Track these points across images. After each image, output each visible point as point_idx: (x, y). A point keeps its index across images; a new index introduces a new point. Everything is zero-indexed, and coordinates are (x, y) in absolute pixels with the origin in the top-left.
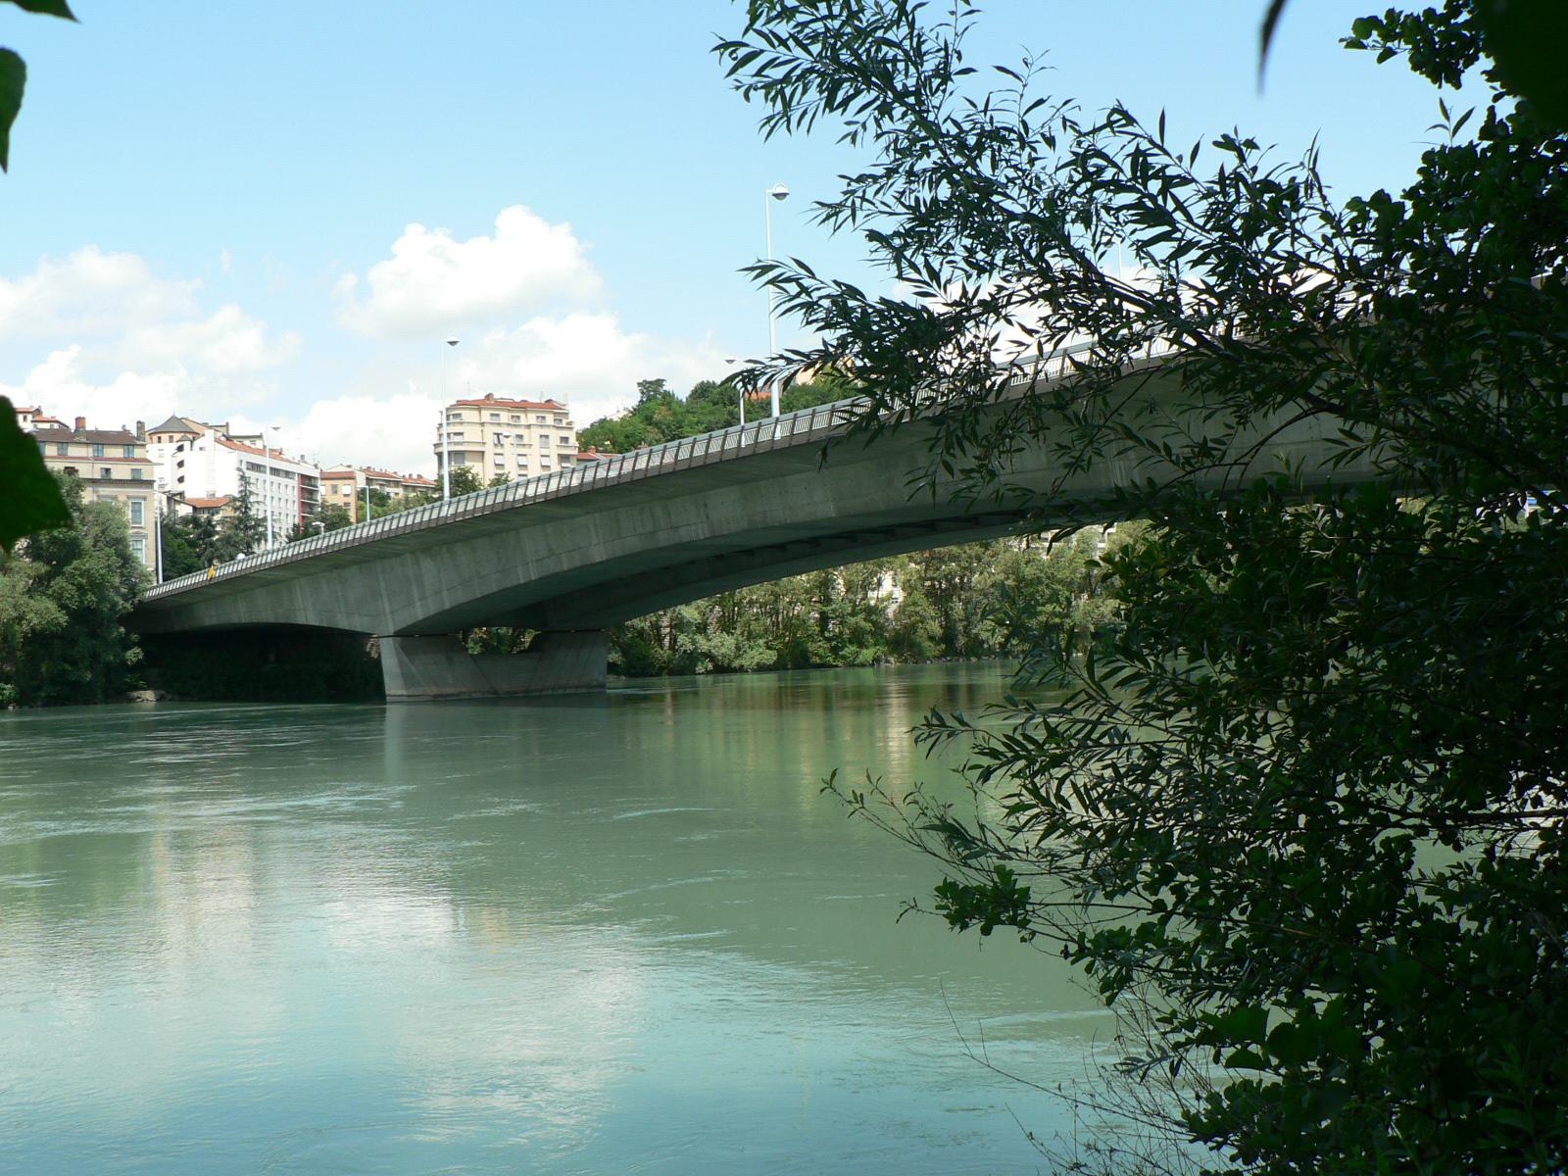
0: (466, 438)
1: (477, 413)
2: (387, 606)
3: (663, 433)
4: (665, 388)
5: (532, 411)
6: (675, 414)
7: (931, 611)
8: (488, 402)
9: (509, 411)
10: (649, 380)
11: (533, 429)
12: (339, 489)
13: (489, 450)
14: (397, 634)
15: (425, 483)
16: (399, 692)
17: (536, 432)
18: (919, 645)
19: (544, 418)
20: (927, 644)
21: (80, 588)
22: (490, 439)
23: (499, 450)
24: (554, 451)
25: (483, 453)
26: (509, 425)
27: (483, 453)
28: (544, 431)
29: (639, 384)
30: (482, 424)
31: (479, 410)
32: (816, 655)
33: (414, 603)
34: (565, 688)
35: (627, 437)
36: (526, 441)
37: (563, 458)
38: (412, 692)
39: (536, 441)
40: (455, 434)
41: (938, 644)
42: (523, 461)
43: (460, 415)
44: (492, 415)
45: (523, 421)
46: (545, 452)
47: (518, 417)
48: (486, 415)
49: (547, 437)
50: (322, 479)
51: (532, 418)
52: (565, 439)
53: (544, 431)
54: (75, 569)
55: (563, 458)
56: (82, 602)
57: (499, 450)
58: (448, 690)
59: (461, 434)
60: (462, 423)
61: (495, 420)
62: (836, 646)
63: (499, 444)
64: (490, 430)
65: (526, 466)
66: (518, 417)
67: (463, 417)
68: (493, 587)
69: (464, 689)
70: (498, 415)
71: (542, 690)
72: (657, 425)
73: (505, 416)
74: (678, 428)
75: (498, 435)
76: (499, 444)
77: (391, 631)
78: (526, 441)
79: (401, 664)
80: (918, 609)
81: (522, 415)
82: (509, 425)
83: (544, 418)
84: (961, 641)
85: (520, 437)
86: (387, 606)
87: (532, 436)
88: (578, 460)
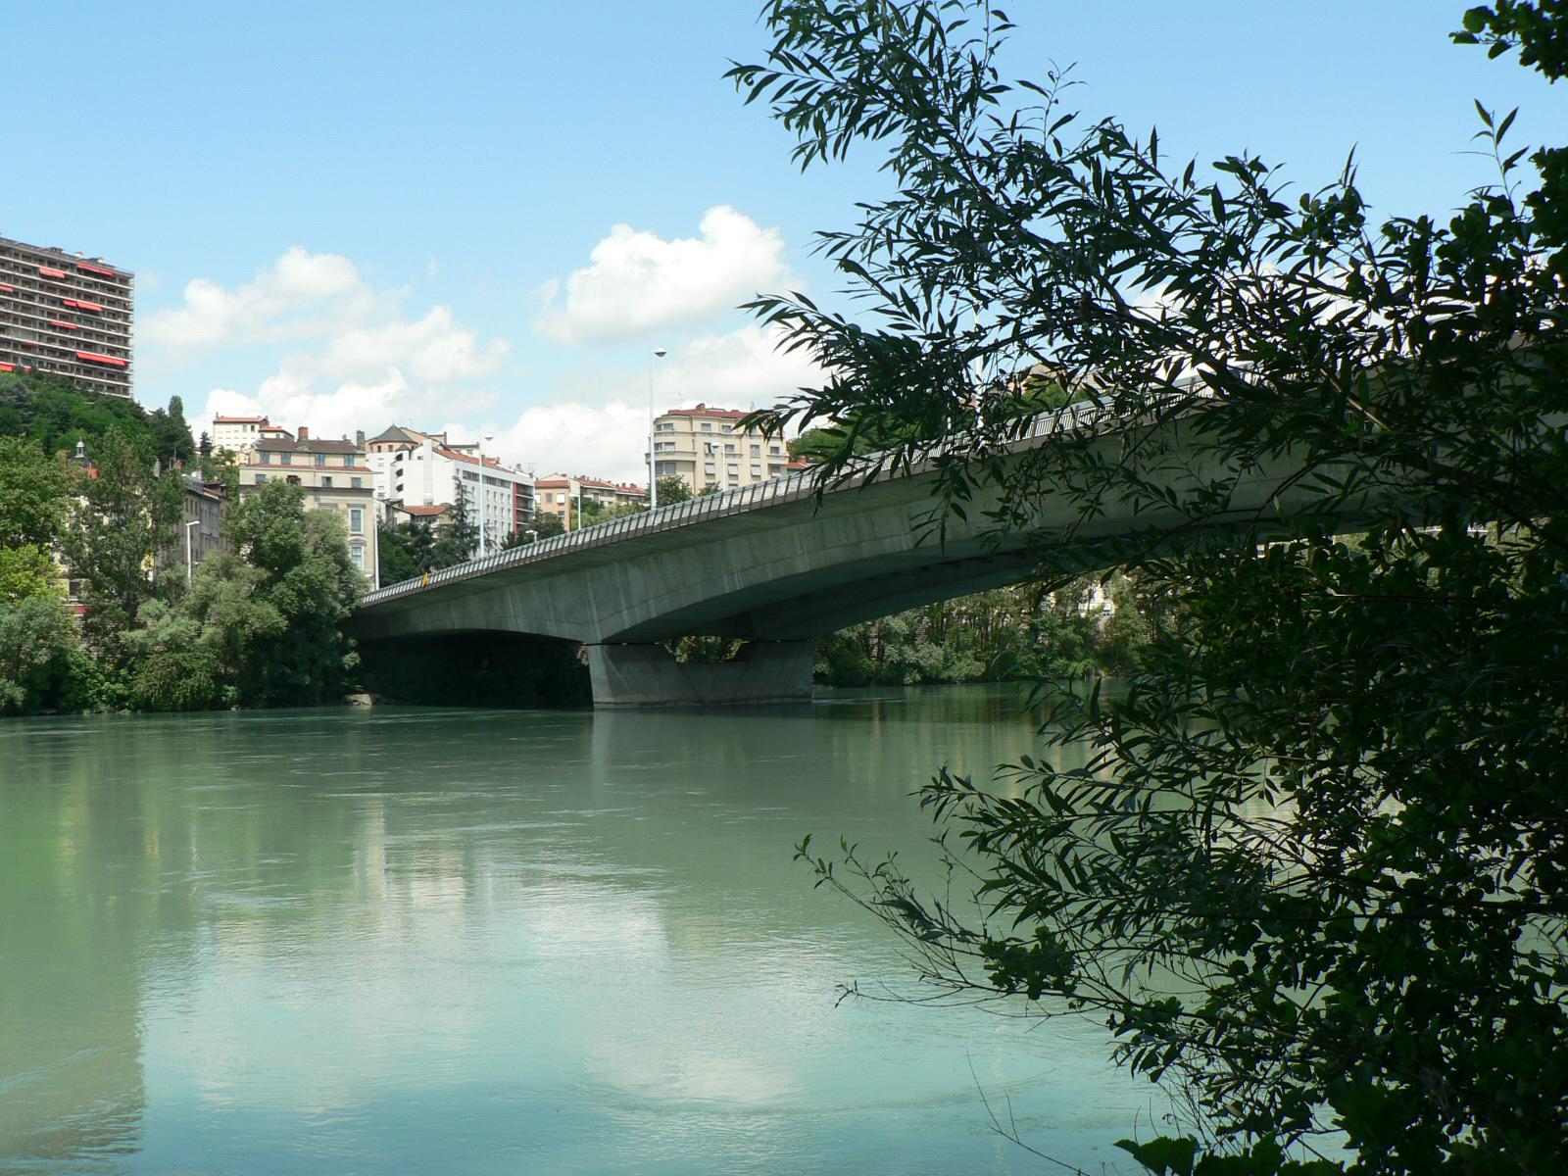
0: (678, 448)
1: (688, 423)
5: (698, 419)
9: (720, 421)
13: (700, 460)
22: (701, 448)
23: (710, 460)
24: (764, 461)
26: (719, 434)
30: (694, 434)
31: (691, 420)
37: (773, 468)
40: (667, 444)
42: (733, 470)
44: (703, 425)
46: (756, 461)
48: (697, 425)
49: (758, 447)
56: (301, 607)
57: (710, 460)
58: (654, 698)
59: (673, 444)
64: (701, 440)
69: (667, 697)
76: (710, 453)
77: (600, 639)
79: (608, 672)
82: (719, 434)
85: (732, 446)
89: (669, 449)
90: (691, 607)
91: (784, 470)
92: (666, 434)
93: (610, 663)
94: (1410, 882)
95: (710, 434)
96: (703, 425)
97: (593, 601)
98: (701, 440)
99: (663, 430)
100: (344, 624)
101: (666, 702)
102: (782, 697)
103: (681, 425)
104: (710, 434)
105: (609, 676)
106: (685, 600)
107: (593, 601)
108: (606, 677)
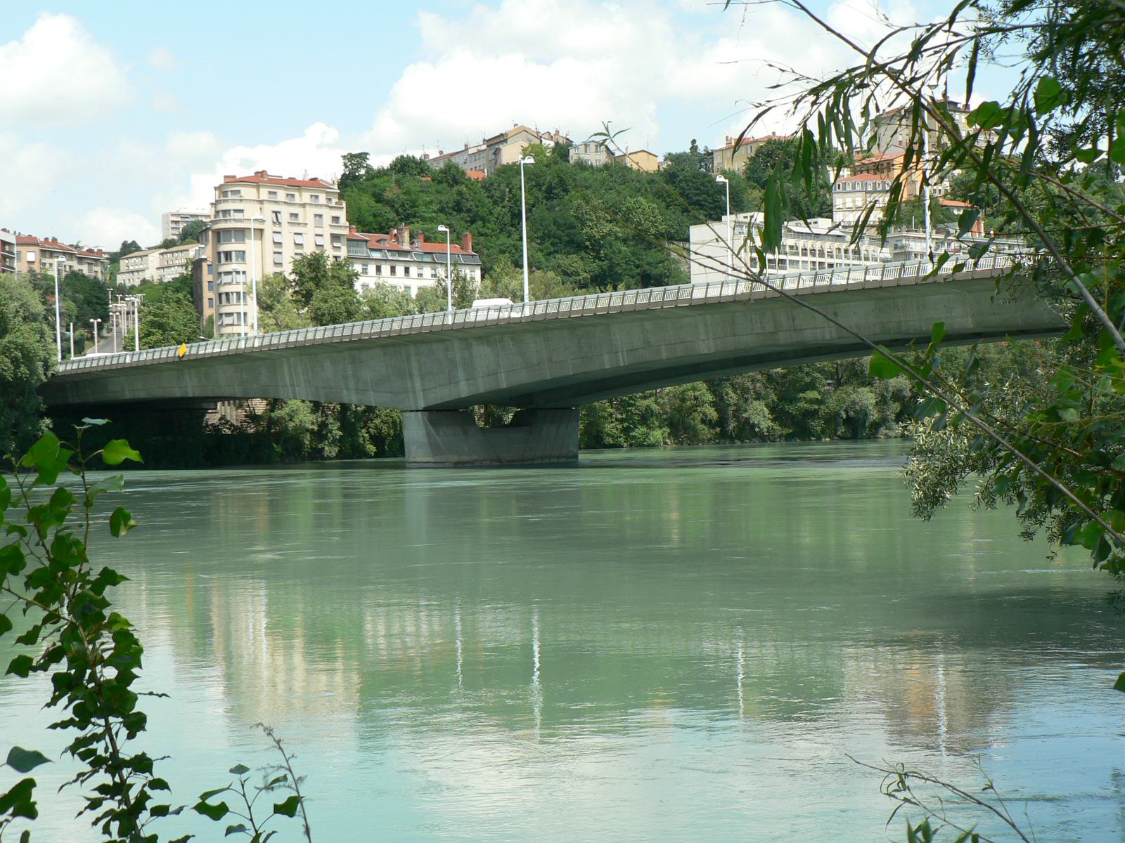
0: (246, 215)
1: (254, 190)
2: (418, 385)
3: (397, 212)
4: (368, 162)
5: (265, 186)
6: (407, 193)
7: (709, 397)
8: (259, 179)
9: (285, 189)
10: (353, 153)
11: (308, 208)
12: (23, 255)
13: (268, 228)
14: (425, 410)
15: (62, 248)
16: (425, 459)
17: (311, 211)
18: (694, 428)
19: (317, 197)
20: (701, 426)
21: (15, 361)
22: (269, 217)
23: (277, 229)
24: (327, 231)
25: (262, 231)
26: (285, 203)
27: (262, 231)
28: (318, 211)
29: (344, 157)
30: (261, 202)
31: (258, 187)
32: (608, 435)
33: (457, 382)
34: (559, 457)
35: (375, 216)
36: (301, 220)
37: (335, 237)
38: (438, 459)
39: (311, 220)
40: (236, 211)
41: (714, 428)
42: (299, 240)
43: (239, 191)
44: (270, 193)
45: (297, 200)
46: (319, 231)
47: (293, 196)
48: (264, 194)
49: (320, 216)
50: (18, 245)
51: (306, 197)
52: (336, 219)
53: (318, 211)
54: (10, 342)
55: (335, 237)
56: (16, 374)
57: (277, 229)
58: (465, 458)
59: (241, 211)
60: (241, 200)
61: (273, 198)
62: (628, 428)
63: (277, 222)
64: (269, 208)
65: (302, 245)
66: (293, 196)
67: (242, 194)
68: (569, 371)
69: (476, 458)
70: (275, 193)
71: (533, 460)
72: (390, 204)
73: (281, 195)
74: (412, 207)
75: (276, 213)
76: (277, 222)
77: (422, 405)
78: (301, 220)
79: (428, 435)
80: (697, 393)
81: (297, 194)
82: (285, 203)
83: (317, 197)
84: (732, 425)
85: (296, 215)
86: (418, 385)
87: (307, 215)
88: (348, 240)
89: (238, 216)
90: (560, 378)
91: (344, 240)
92: (233, 201)
93: (431, 428)
94: (92, 744)
95: (276, 202)
96: (288, 195)
97: (416, 373)
98: (269, 208)
99: (230, 196)
100: (44, 389)
101: (475, 461)
102: (559, 457)
103: (248, 192)
104: (276, 202)
105: (429, 440)
106: (548, 374)
107: (416, 373)
108: (426, 440)
